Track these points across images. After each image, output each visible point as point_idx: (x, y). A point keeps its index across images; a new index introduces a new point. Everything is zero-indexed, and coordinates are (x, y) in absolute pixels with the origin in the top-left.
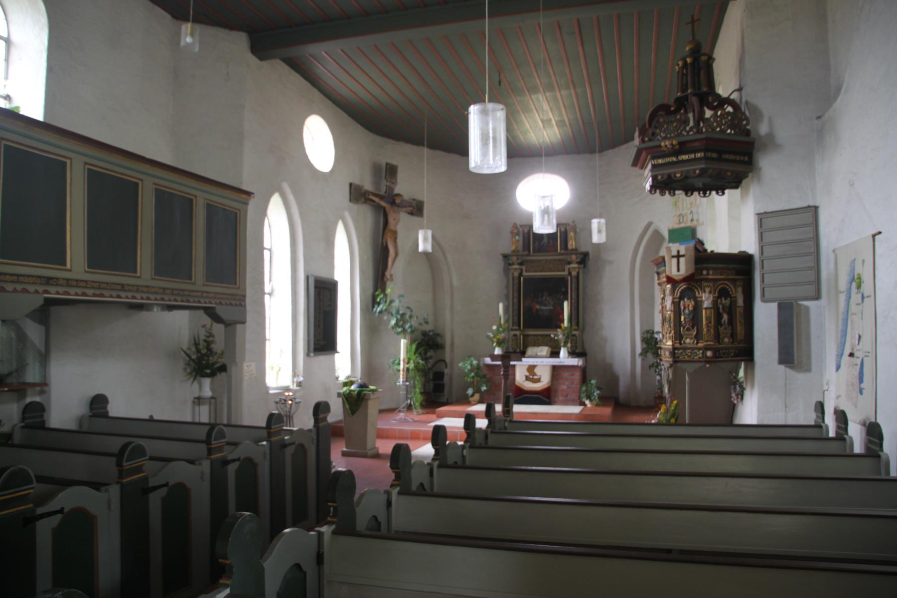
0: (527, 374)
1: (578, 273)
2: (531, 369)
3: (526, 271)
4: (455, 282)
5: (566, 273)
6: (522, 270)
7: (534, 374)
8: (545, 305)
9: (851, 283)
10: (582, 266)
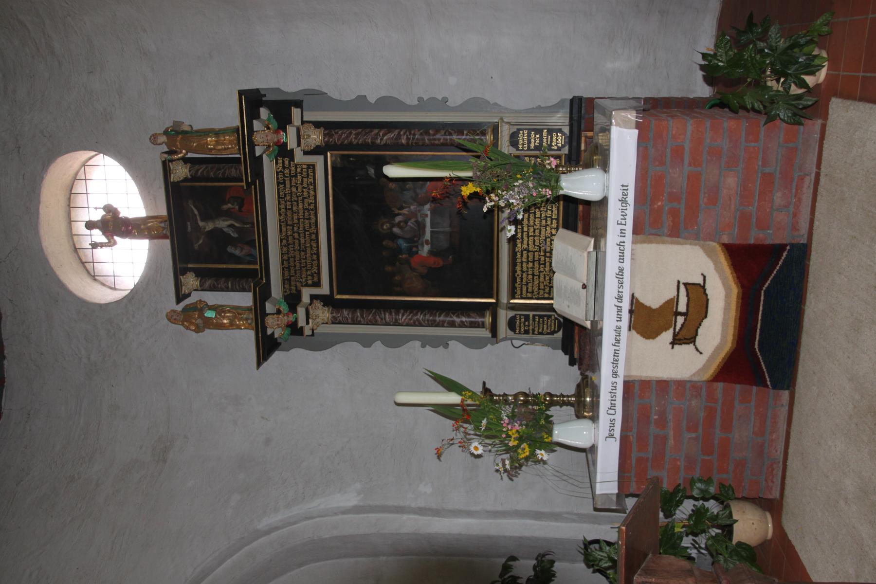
0: (591, 570)
1: (317, 125)
2: (645, 320)
3: (318, 284)
4: (351, 499)
5: (318, 160)
6: (313, 297)
7: (670, 306)
8: (421, 226)
9: (175, 160)
10: (296, 112)
